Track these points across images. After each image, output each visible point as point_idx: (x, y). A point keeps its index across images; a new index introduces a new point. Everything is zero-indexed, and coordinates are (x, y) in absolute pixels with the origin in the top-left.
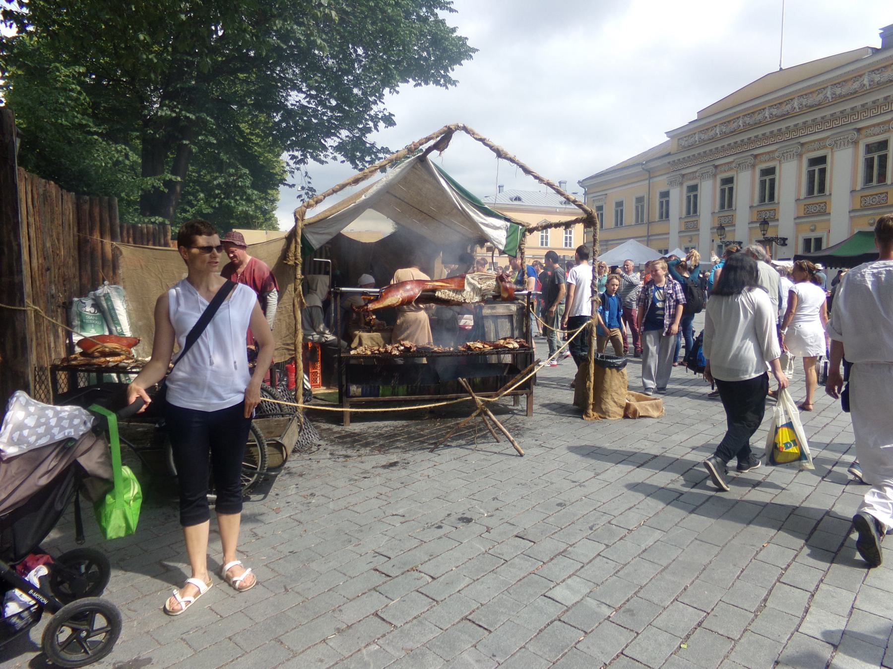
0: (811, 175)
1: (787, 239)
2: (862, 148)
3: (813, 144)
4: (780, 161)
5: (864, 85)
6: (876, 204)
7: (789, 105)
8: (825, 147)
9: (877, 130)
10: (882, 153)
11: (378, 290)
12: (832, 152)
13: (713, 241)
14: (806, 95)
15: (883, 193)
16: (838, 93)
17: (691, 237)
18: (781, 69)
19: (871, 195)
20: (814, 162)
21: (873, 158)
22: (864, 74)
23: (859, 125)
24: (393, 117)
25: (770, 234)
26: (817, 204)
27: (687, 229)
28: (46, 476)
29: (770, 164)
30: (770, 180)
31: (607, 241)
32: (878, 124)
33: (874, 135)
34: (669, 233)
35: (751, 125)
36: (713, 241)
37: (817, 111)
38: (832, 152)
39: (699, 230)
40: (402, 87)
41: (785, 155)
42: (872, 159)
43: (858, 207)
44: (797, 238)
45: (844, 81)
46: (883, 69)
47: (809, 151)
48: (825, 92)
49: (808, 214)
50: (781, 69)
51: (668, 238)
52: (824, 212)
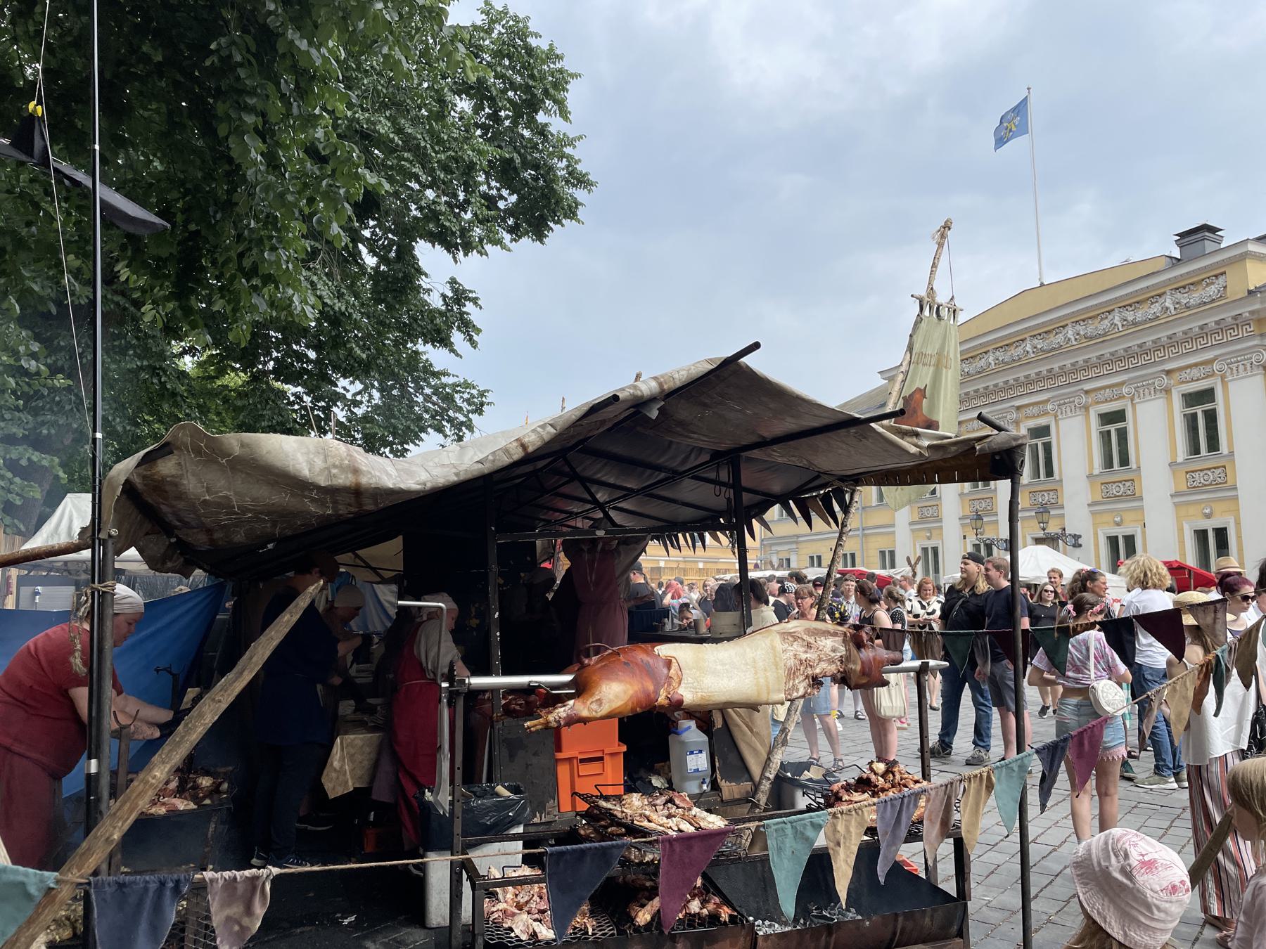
0: (1191, 421)
1: (1080, 536)
2: (1177, 402)
3: (1102, 392)
4: (1056, 416)
5: (1167, 308)
6: (1210, 485)
7: (1106, 322)
8: (1121, 397)
9: (1195, 373)
10: (1207, 407)
11: (567, 678)
12: (1133, 405)
13: (965, 537)
14: (1084, 320)
15: (1218, 468)
16: (1130, 319)
17: (929, 530)
18: (1042, 285)
19: (1201, 470)
20: (1193, 399)
21: (1196, 413)
22: (1165, 293)
23: (1168, 367)
24: (469, 307)
25: (1053, 529)
26: (1120, 482)
27: (923, 519)
28: (513, 475)
29: (1042, 421)
30: (1044, 444)
31: (798, 536)
32: (1196, 365)
33: (1106, 401)
34: (893, 525)
35: (1007, 363)
36: (965, 537)
37: (1137, 334)
38: (1133, 405)
39: (941, 521)
40: (452, 340)
41: (1234, 366)
42: (1194, 416)
43: (1100, 499)
44: (1096, 534)
45: (1192, 284)
46: (1191, 287)
47: (1098, 403)
48: (1110, 317)
49: (1109, 499)
50: (1042, 285)
51: (893, 533)
52: (1133, 496)
